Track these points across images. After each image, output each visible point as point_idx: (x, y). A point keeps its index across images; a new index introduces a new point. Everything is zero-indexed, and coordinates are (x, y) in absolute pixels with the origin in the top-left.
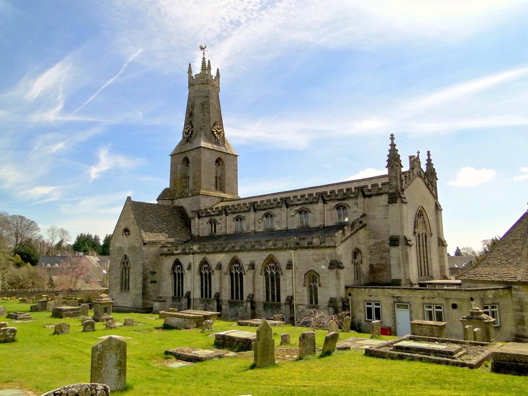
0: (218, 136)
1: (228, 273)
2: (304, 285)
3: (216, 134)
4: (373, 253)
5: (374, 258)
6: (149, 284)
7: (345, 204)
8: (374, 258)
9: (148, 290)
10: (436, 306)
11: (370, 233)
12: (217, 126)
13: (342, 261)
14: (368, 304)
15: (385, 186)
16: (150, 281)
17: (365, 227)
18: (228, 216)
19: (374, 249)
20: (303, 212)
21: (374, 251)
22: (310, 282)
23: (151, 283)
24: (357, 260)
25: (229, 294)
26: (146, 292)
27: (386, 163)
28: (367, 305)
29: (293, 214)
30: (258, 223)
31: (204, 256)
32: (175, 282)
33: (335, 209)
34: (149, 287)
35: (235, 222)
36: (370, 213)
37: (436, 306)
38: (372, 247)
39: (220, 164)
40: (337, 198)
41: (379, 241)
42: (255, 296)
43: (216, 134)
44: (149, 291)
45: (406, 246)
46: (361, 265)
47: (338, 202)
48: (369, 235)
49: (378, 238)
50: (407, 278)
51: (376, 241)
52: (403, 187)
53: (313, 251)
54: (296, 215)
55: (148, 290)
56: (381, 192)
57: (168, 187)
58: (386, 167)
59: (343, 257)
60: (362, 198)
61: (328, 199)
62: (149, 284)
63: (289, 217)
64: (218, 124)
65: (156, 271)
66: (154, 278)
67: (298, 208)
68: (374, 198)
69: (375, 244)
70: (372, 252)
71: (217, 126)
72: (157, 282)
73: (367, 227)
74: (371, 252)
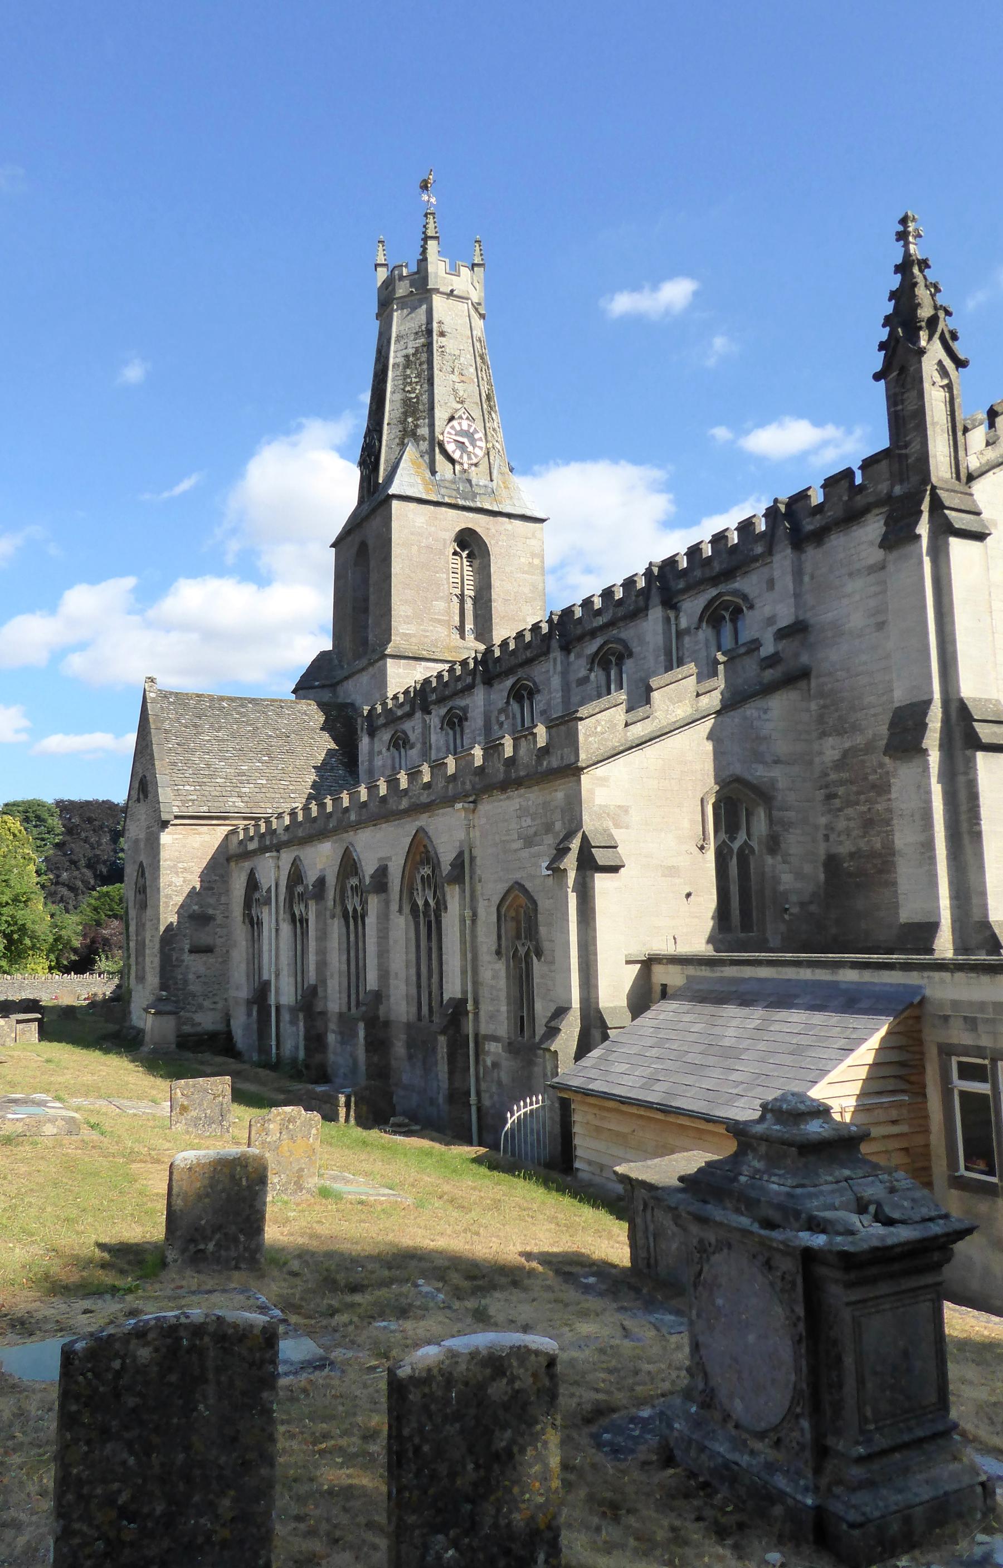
0: (461, 457)
1: (338, 910)
2: (498, 953)
3: (454, 452)
4: (837, 803)
5: (841, 824)
6: (187, 957)
7: (735, 593)
8: (841, 824)
9: (180, 977)
10: (960, 1063)
11: (824, 707)
12: (460, 424)
13: (619, 835)
14: (968, 1072)
15: (876, 467)
16: (187, 947)
17: (803, 684)
18: (429, 713)
19: (842, 783)
20: (613, 659)
21: (841, 791)
22: (518, 937)
23: (191, 951)
24: (742, 837)
25: (340, 992)
26: (176, 983)
27: (877, 361)
28: (962, 1076)
29: (583, 673)
30: (496, 727)
31: (296, 853)
32: (521, 987)
33: (704, 625)
34: (185, 964)
35: (447, 734)
36: (824, 615)
37: (960, 1063)
38: (833, 776)
39: (476, 553)
40: (708, 574)
41: (859, 740)
42: (388, 996)
43: (454, 452)
44: (186, 981)
45: (968, 752)
46: (769, 860)
47: (713, 592)
48: (821, 719)
49: (855, 728)
50: (976, 917)
51: (847, 745)
52: (973, 462)
53: (520, 796)
54: (593, 676)
55: (180, 977)
56: (860, 501)
57: (328, 645)
58: (877, 377)
59: (635, 817)
60: (789, 551)
61: (681, 585)
62: (187, 957)
63: (574, 685)
64: (460, 417)
65: (211, 911)
66: (204, 938)
67: (592, 647)
68: (837, 541)
69: (845, 754)
70: (835, 796)
71: (460, 424)
72: (217, 949)
73: (813, 683)
74: (830, 797)
